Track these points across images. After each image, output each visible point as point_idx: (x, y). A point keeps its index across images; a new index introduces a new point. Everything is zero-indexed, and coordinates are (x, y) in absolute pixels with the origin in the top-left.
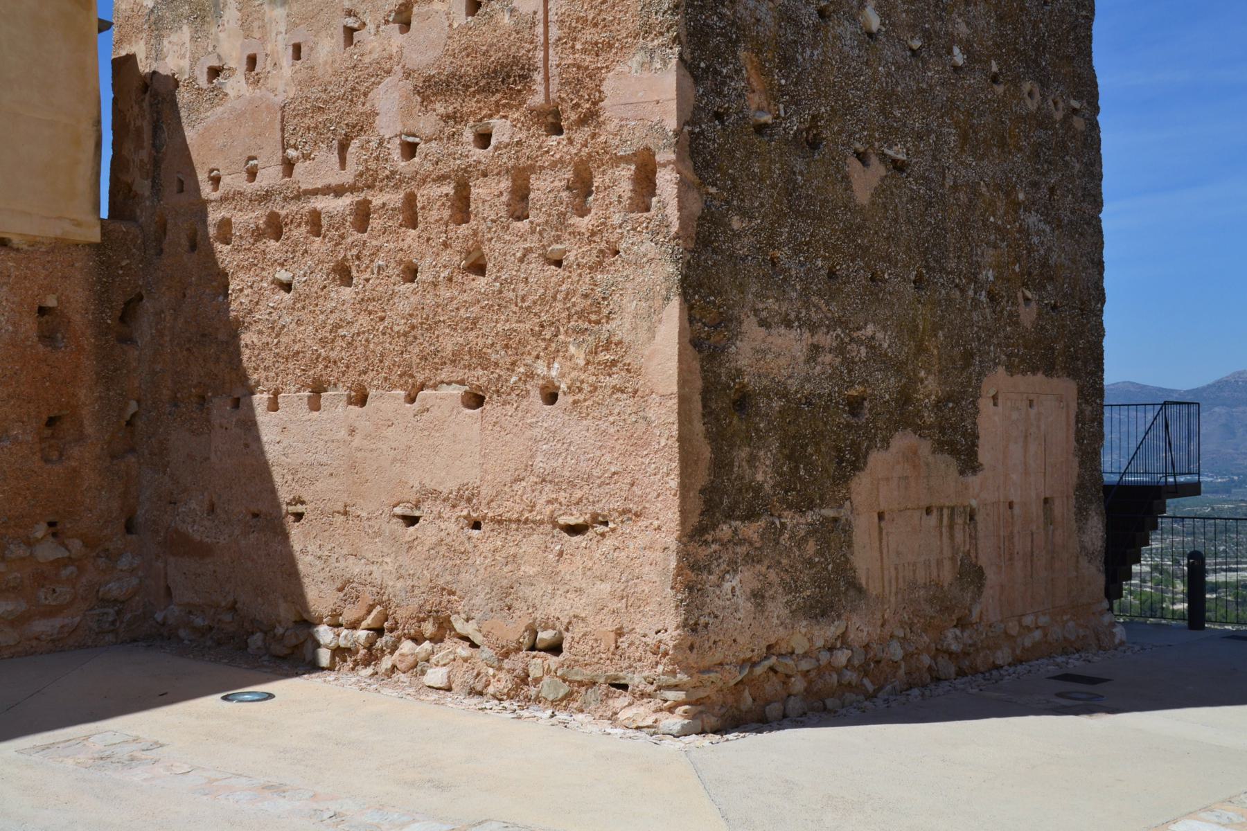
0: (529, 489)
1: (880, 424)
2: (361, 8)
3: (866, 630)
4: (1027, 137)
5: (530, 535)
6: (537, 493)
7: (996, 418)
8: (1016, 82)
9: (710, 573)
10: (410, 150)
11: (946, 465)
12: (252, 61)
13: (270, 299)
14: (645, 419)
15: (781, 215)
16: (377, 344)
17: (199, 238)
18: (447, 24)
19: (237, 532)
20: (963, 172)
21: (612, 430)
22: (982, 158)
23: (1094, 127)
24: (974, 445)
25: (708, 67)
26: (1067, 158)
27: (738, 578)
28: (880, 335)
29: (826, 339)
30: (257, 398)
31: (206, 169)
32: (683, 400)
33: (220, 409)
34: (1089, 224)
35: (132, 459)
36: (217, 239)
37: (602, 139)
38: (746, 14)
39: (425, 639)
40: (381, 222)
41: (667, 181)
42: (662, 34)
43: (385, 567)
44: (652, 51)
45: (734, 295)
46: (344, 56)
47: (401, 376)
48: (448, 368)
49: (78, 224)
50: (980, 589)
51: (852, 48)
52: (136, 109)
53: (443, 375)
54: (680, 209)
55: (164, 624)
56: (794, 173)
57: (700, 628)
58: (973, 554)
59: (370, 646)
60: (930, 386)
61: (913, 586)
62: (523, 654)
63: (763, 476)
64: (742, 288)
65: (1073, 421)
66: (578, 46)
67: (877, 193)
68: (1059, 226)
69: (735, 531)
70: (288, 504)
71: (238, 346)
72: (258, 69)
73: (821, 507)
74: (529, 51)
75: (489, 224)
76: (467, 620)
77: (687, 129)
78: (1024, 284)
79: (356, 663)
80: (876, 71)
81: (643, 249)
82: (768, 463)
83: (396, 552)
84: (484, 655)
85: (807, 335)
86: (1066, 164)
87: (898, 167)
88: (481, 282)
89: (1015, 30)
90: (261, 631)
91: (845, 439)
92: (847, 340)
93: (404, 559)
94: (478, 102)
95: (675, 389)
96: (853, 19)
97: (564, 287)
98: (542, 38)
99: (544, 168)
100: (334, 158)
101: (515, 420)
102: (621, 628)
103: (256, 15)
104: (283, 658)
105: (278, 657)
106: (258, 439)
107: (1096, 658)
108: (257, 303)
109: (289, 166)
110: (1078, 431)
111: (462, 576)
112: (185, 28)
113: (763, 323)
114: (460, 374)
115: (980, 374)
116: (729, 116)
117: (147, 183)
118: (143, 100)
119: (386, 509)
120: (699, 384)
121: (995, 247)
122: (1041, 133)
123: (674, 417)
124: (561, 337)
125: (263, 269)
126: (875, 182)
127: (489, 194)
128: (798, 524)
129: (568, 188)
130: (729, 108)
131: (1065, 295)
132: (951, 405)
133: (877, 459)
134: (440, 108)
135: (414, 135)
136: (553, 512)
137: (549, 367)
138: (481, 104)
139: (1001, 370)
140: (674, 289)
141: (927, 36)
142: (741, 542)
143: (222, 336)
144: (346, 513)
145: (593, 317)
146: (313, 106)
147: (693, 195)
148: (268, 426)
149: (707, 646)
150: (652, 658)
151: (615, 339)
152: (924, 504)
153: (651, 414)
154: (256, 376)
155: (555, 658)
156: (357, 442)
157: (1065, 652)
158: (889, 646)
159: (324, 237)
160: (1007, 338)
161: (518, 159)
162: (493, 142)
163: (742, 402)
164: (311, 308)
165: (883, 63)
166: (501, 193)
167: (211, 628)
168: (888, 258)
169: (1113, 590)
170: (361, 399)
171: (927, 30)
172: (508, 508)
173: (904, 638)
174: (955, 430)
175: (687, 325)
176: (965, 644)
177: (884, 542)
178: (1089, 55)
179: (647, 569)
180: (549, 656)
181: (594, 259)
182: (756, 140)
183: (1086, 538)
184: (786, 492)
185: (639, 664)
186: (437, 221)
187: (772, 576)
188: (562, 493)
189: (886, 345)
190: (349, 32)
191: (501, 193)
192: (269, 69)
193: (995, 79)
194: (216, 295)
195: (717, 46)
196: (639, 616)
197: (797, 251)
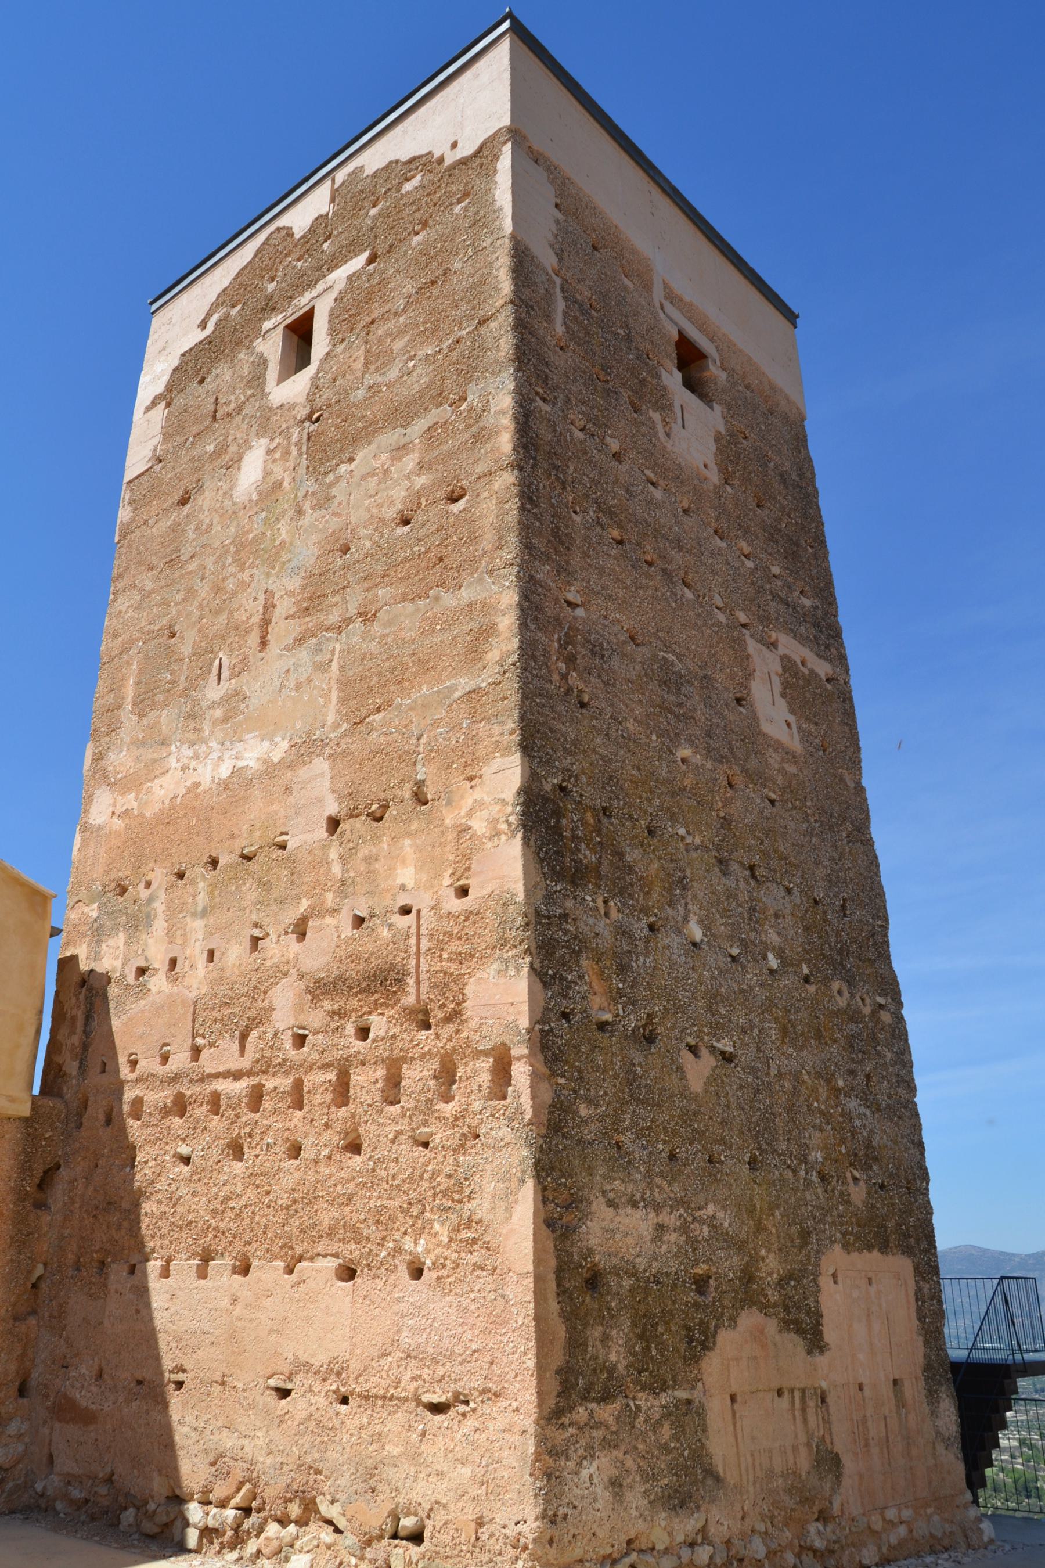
0: (394, 1365)
1: (726, 1303)
2: (265, 921)
3: (726, 1523)
4: (841, 1030)
5: (395, 1412)
6: (402, 1369)
7: (838, 1297)
8: (826, 982)
9: (568, 1459)
10: (300, 1041)
11: (794, 1344)
12: (173, 963)
13: (171, 1173)
14: (503, 1296)
15: (624, 1103)
16: (262, 1217)
17: (114, 1114)
18: (336, 935)
19: (121, 1399)
20: (786, 1062)
21: (473, 1307)
22: (802, 1048)
23: (900, 1020)
24: (819, 1324)
25: (555, 974)
26: (879, 1048)
27: (595, 1464)
28: (720, 1215)
29: (670, 1219)
30: (151, 1264)
31: (127, 1053)
32: (538, 1279)
33: (117, 1272)
34: (905, 1107)
35: (32, 1321)
36: (130, 1115)
37: (465, 1035)
38: (586, 929)
39: (291, 1522)
40: (272, 1103)
41: (521, 1073)
42: (515, 947)
43: (257, 1442)
44: (507, 961)
45: (583, 1178)
46: (251, 961)
47: (281, 1248)
48: (325, 1241)
49: (12, 1100)
50: (838, 1477)
51: (679, 956)
52: (74, 1000)
53: (320, 1249)
54: (533, 1098)
55: (42, 1495)
56: (634, 1065)
57: (559, 1520)
58: (828, 1441)
59: (237, 1528)
60: (771, 1266)
61: (770, 1474)
62: (385, 1542)
63: (616, 1356)
64: (590, 1171)
65: (912, 1299)
66: (445, 956)
67: (710, 1081)
68: (879, 1110)
69: (591, 1414)
70: (171, 1372)
71: (139, 1215)
72: (177, 969)
73: (673, 1388)
74: (403, 959)
75: (366, 1108)
76: (332, 1502)
77: (538, 1027)
78: (851, 1165)
79: (222, 1546)
80: (701, 975)
81: (500, 1134)
82: (620, 1342)
83: (268, 1426)
84: (348, 1542)
85: (652, 1214)
86: (878, 1053)
87: (727, 1058)
88: (357, 1161)
89: (820, 938)
90: (134, 1506)
91: (694, 1318)
92: (690, 1219)
93: (275, 1434)
94: (359, 1001)
95: (530, 1267)
96: (679, 931)
97: (430, 1168)
98: (414, 949)
99: (415, 1059)
100: (236, 1046)
101: (384, 1294)
102: (481, 1517)
103: (179, 926)
104: (152, 1537)
105: (148, 1536)
106: (148, 1305)
107: (966, 1560)
108: (159, 1175)
109: (196, 1052)
110: (919, 1309)
111: (329, 1453)
112: (121, 935)
113: (611, 1204)
114: (335, 1247)
115: (818, 1252)
116: (575, 1015)
117: (76, 1064)
118: (80, 993)
119: (261, 1381)
120: (553, 1263)
121: (821, 1130)
122: (853, 1026)
123: (530, 1296)
124: (427, 1215)
125: (167, 1143)
126: (707, 1072)
127: (366, 1081)
128: (652, 1406)
129: (435, 1077)
130: (574, 1009)
131: (891, 1175)
132: (792, 1283)
133: (725, 1338)
134: (327, 1005)
135: (304, 1028)
136: (417, 1389)
137: (416, 1244)
138: (362, 1003)
139: (837, 1248)
140: (529, 1172)
141: (744, 944)
142: (599, 1425)
143: (125, 1205)
144: (223, 1383)
145: (456, 1196)
146: (221, 1001)
147: (544, 1086)
148: (159, 1291)
149: (566, 1540)
150: (511, 1553)
151: (476, 1218)
152: (775, 1385)
153: (509, 1292)
154: (152, 1244)
155: (416, 1549)
156: (238, 1311)
157: (933, 1551)
158: (750, 1542)
159: (222, 1116)
160: (840, 1216)
161: (392, 1050)
162: (371, 1035)
163: (594, 1281)
164: (206, 1181)
165: (707, 967)
166: (377, 1080)
167: (87, 1501)
168: (723, 1141)
169: (975, 1481)
170: (244, 1269)
171: (743, 940)
172: (375, 1384)
173: (766, 1533)
174: (799, 1308)
175: (541, 1206)
176: (828, 1541)
177: (738, 1425)
178: (888, 957)
179: (506, 1453)
180: (410, 1545)
181: (457, 1142)
182: (598, 1035)
183: (940, 1423)
184: (639, 1373)
185: (499, 1558)
186: (320, 1104)
187: (629, 1463)
188: (426, 1370)
189: (726, 1225)
190: (255, 940)
191: (377, 1080)
192: (186, 969)
193: (807, 980)
194: (123, 1167)
195: (563, 956)
196: (499, 1504)
197: (639, 1135)
